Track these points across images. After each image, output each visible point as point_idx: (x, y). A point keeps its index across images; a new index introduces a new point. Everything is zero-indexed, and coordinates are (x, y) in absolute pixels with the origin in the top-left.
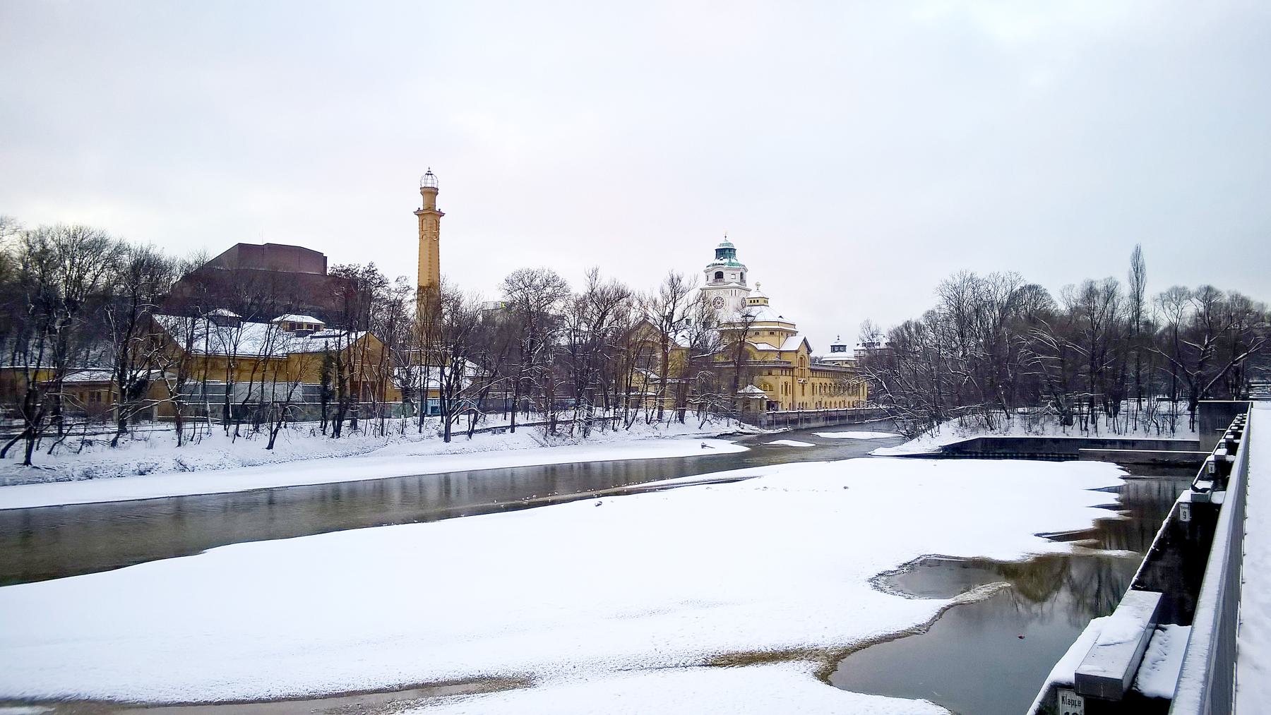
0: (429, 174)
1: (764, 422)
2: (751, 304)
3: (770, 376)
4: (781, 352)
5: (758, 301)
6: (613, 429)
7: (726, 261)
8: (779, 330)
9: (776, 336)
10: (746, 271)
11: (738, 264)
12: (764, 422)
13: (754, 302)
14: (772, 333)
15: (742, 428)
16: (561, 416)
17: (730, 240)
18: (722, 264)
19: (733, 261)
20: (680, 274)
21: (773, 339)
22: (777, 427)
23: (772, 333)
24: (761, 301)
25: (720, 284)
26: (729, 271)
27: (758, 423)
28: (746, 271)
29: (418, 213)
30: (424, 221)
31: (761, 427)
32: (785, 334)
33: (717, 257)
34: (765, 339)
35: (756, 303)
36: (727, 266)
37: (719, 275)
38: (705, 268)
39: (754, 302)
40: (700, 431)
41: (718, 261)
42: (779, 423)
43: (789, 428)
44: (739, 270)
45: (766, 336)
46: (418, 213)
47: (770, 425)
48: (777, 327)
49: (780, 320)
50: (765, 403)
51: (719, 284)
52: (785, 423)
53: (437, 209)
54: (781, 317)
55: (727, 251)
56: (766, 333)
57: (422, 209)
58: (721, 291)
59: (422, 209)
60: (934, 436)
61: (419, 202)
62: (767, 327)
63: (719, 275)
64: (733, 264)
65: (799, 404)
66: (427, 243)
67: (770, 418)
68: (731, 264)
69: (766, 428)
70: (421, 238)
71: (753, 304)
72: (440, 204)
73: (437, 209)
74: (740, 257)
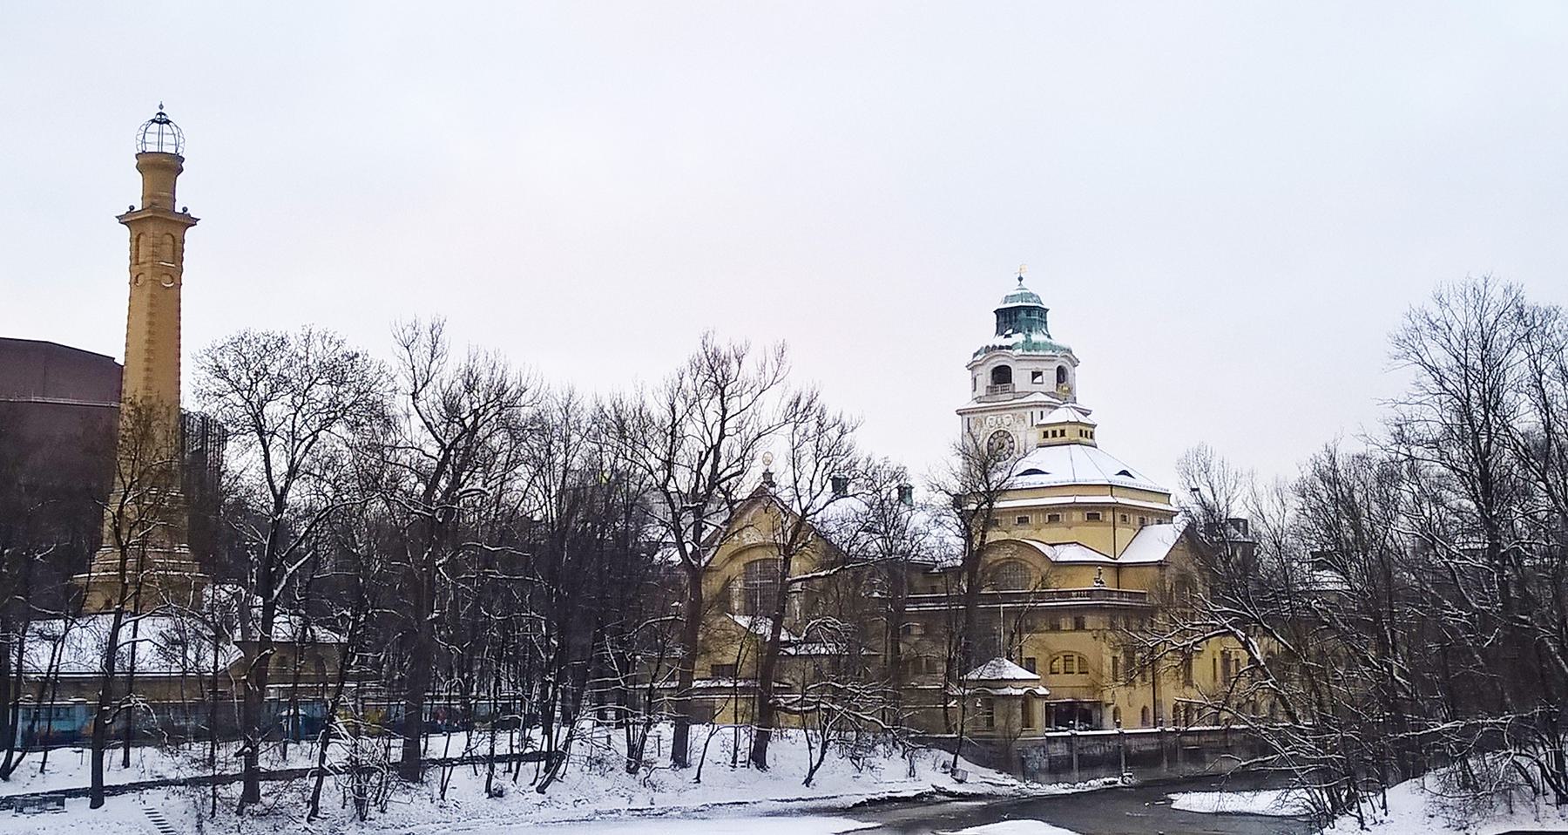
0: (162, 120)
1: (1038, 760)
2: (1047, 441)
3: (1078, 634)
4: (1119, 567)
5: (1063, 433)
6: (488, 790)
7: (1019, 338)
8: (1114, 507)
9: (1107, 524)
10: (1075, 363)
11: (1053, 348)
12: (1038, 760)
13: (1054, 433)
14: (1093, 514)
15: (960, 782)
16: (436, 745)
17: (1030, 286)
18: (1009, 348)
19: (1036, 337)
20: (739, 343)
21: (1097, 533)
22: (1085, 774)
23: (1054, 519)
24: (1071, 433)
25: (1004, 398)
26: (1024, 365)
27: (1019, 765)
28: (1075, 363)
29: (129, 219)
30: (142, 237)
31: (1026, 773)
32: (1134, 520)
33: (999, 332)
34: (1072, 535)
35: (1058, 439)
36: (1020, 351)
37: (1002, 376)
38: (970, 360)
39: (1054, 433)
40: (807, 793)
41: (1001, 341)
42: (1090, 765)
43: (1126, 778)
44: (1051, 359)
45: (1078, 524)
46: (129, 219)
47: (1057, 769)
48: (1109, 499)
49: (1124, 481)
50: (1039, 709)
51: (1001, 397)
52: (1111, 763)
53: (179, 209)
54: (1124, 473)
55: (1023, 314)
56: (1077, 516)
57: (138, 207)
58: (1007, 418)
59: (138, 207)
60: (1368, 823)
61: (131, 192)
62: (1079, 499)
63: (1002, 376)
64: (1036, 346)
65: (1176, 708)
66: (145, 300)
67: (1060, 750)
68: (1029, 345)
69: (1043, 777)
70: (134, 282)
71: (1050, 440)
72: (186, 195)
73: (179, 209)
74: (1060, 330)
